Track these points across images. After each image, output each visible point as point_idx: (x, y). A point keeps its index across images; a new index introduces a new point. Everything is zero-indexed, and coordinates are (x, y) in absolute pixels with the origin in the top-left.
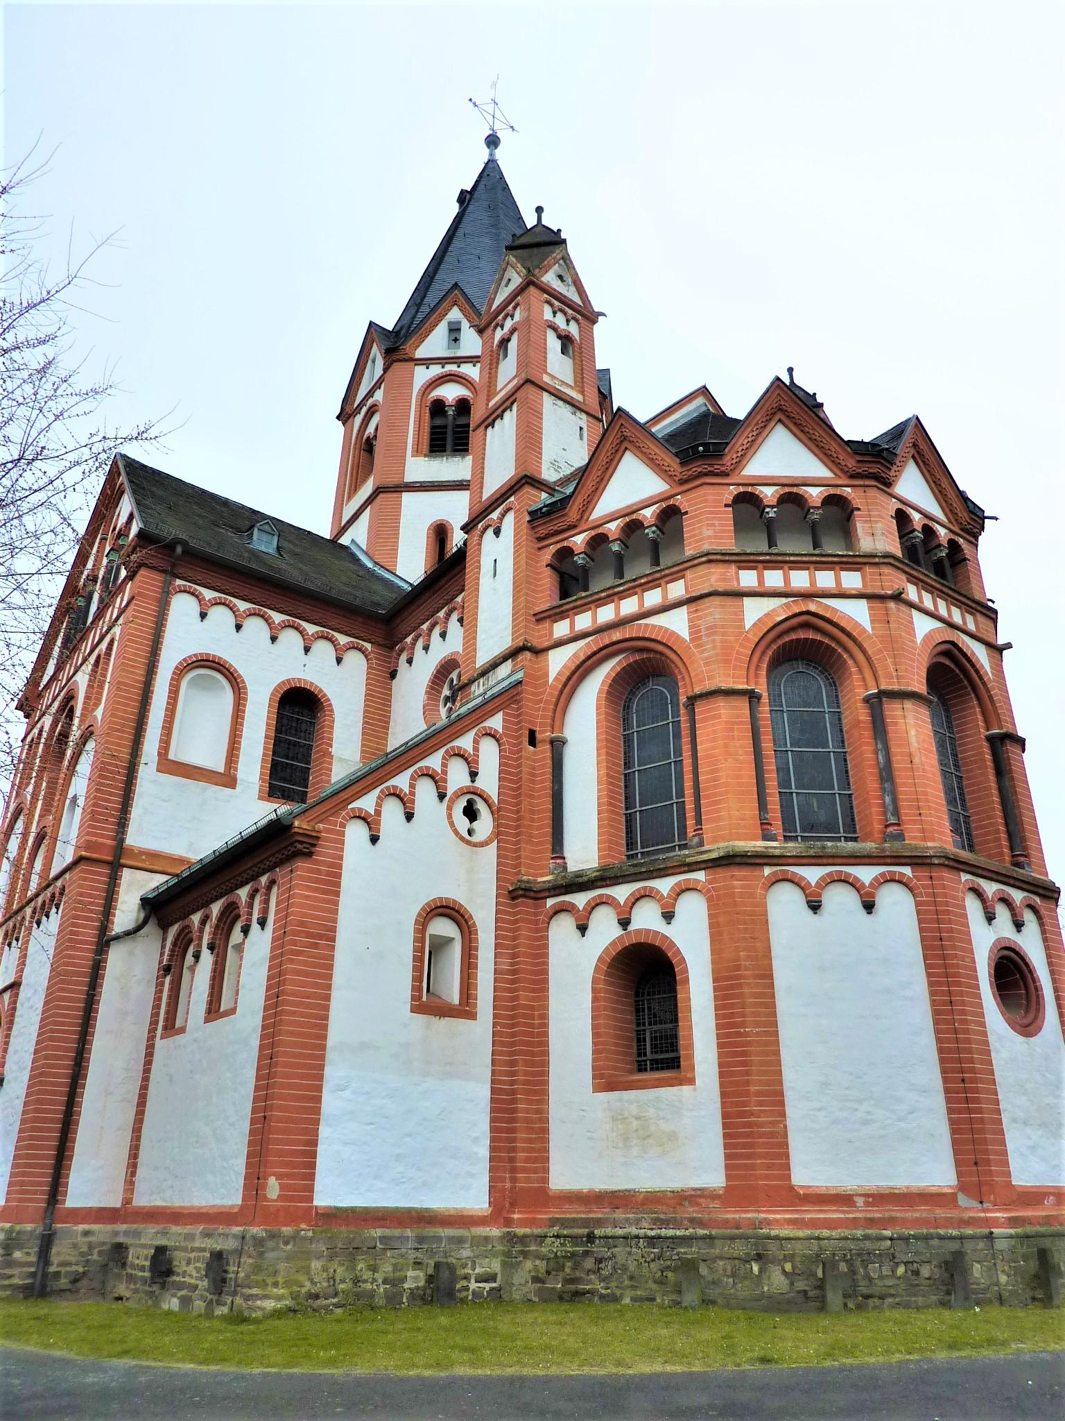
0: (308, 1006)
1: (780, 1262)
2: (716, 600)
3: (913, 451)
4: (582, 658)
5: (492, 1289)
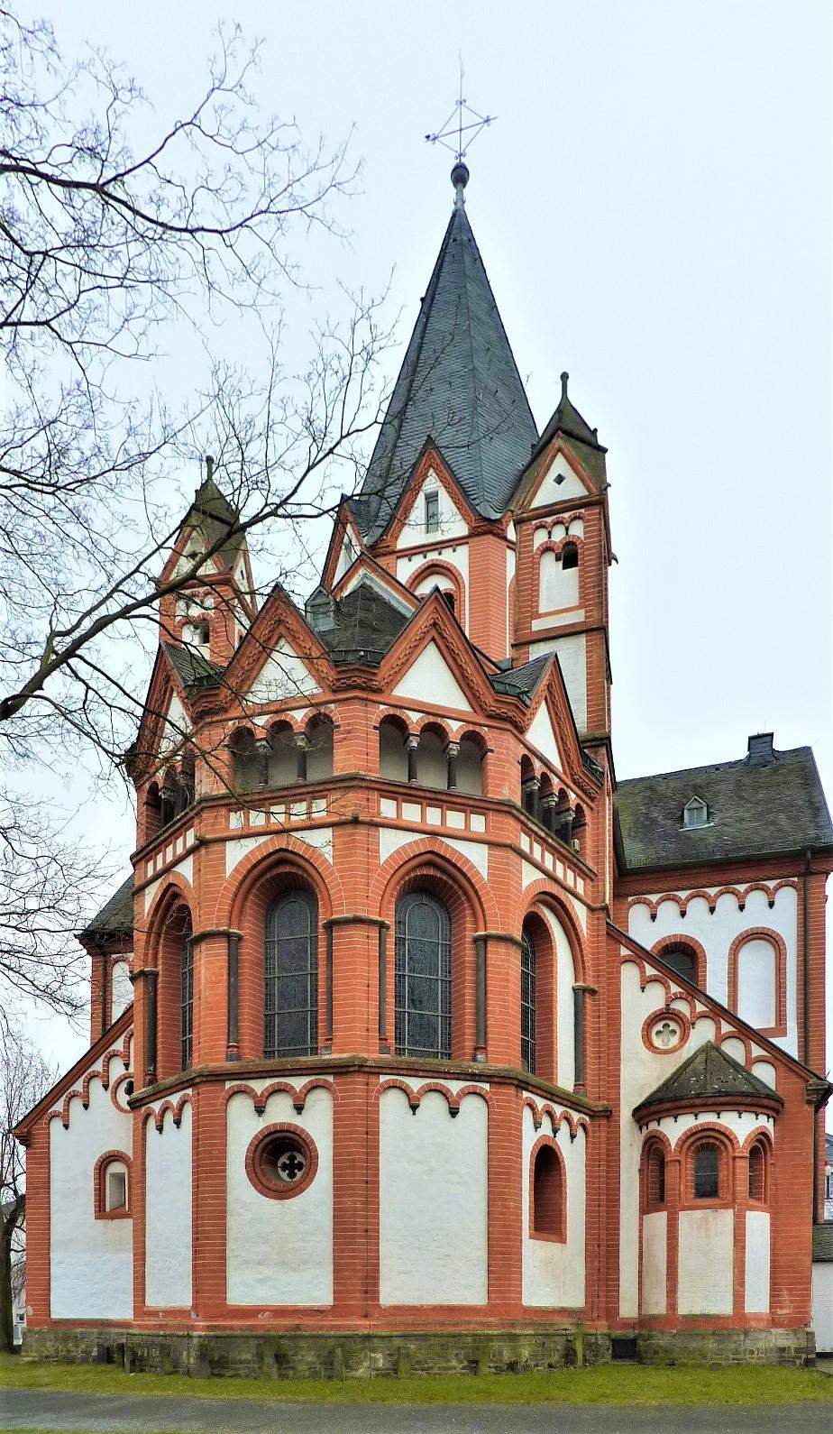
0: (37, 1224)
3: (546, 693)
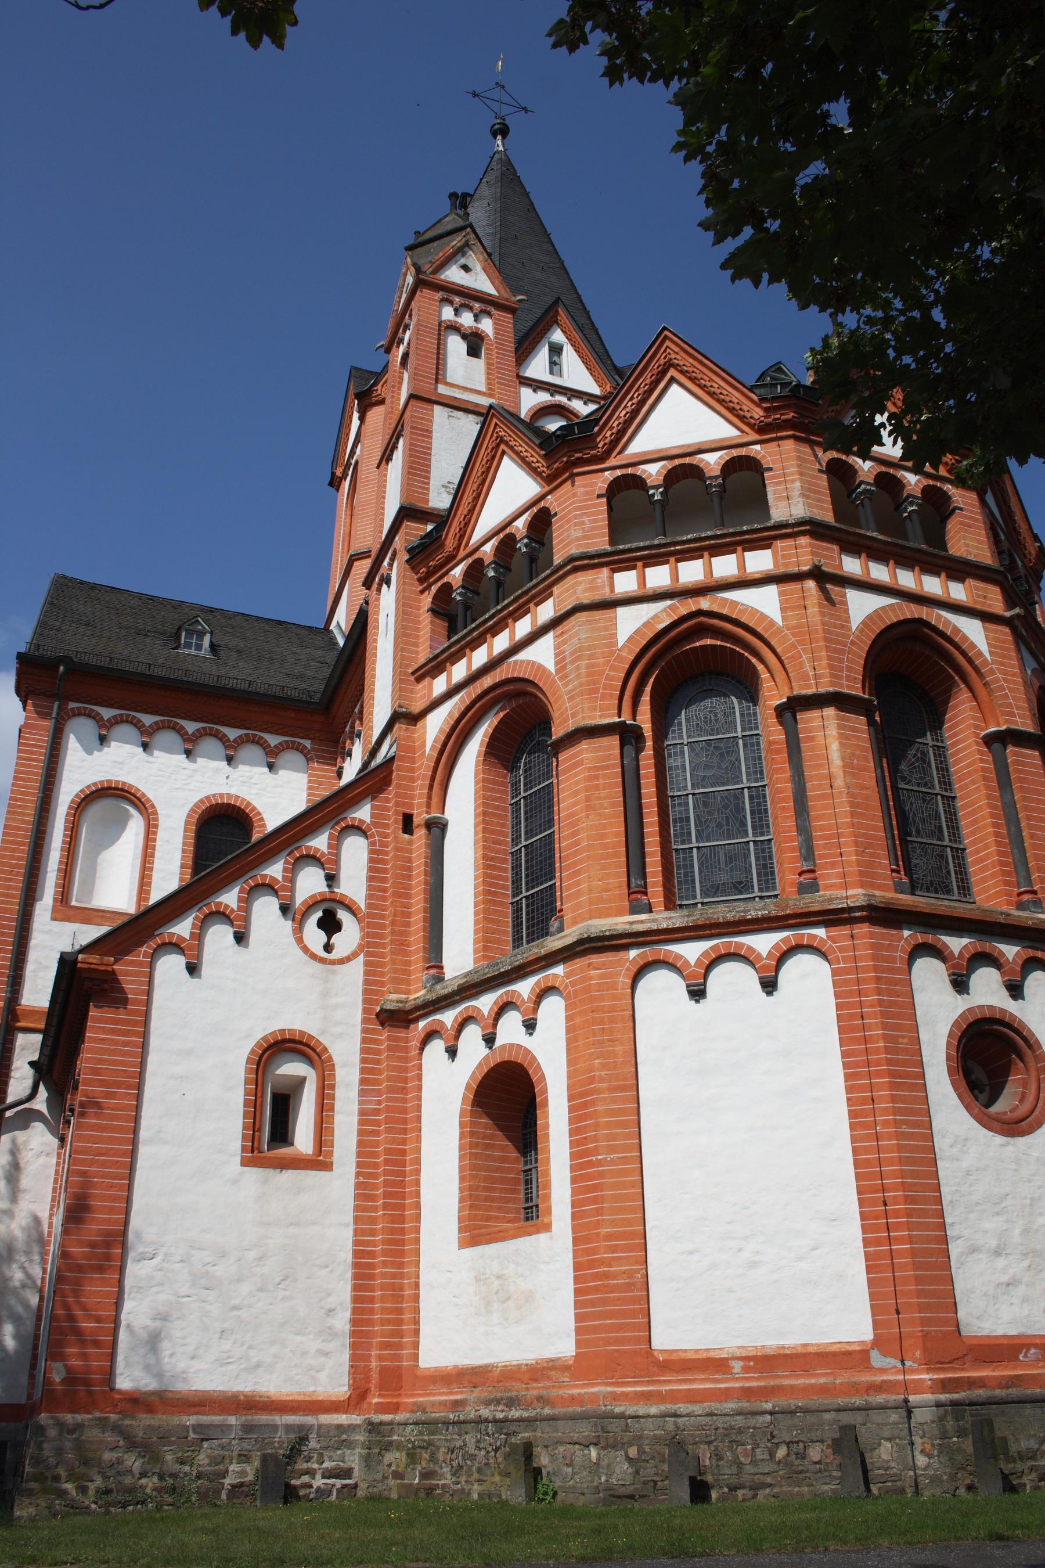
1: (624, 1446)
2: (581, 617)
4: (457, 715)
5: (344, 1486)
